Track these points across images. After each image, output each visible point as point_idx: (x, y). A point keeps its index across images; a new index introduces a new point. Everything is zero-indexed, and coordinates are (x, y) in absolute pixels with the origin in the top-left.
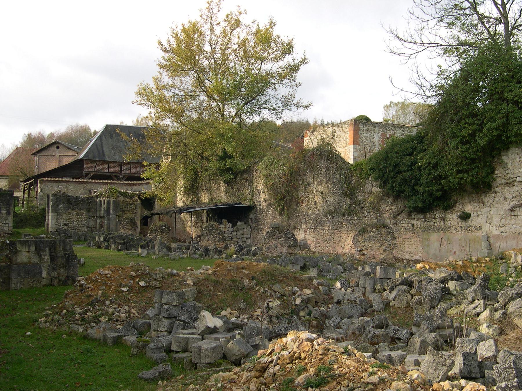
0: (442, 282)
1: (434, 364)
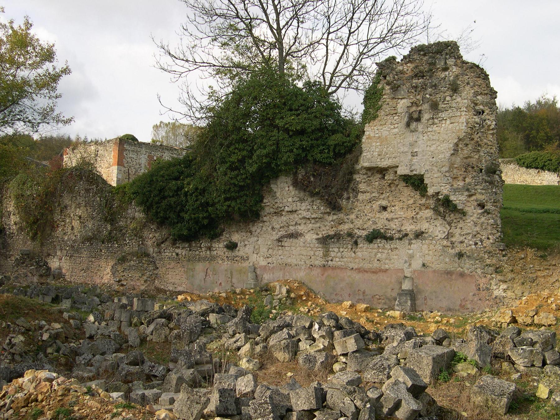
0: (203, 315)
1: (189, 402)
